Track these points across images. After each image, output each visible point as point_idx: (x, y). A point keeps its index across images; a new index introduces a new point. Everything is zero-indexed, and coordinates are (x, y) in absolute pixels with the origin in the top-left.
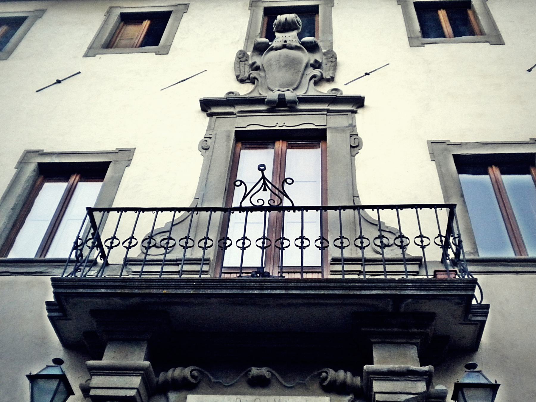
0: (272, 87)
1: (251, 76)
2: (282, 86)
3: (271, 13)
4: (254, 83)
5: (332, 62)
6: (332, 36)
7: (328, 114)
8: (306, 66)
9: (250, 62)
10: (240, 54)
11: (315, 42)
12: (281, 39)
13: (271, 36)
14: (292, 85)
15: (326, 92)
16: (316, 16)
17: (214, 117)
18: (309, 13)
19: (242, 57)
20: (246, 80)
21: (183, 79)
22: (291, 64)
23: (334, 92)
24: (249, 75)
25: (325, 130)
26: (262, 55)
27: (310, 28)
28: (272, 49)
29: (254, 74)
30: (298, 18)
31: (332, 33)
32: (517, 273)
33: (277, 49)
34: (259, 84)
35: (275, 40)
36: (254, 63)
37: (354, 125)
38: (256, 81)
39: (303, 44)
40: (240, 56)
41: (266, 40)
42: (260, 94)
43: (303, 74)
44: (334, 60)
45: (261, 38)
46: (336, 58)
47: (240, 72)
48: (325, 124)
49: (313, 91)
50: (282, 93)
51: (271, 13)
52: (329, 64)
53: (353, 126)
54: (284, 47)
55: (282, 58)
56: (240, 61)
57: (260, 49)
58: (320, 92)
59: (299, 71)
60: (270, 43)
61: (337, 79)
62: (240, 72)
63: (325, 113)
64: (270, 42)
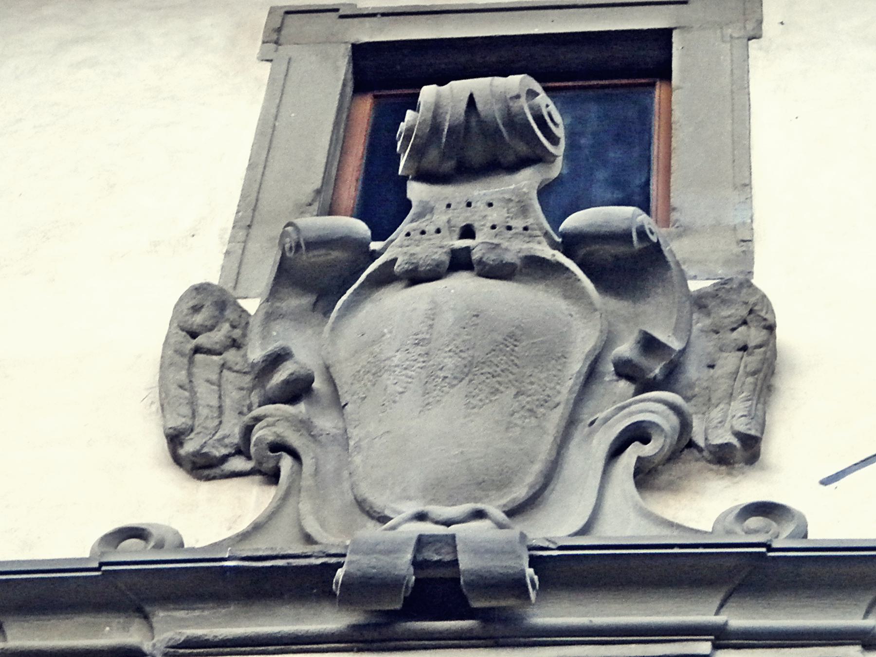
0: (379, 500)
1: (258, 433)
2: (439, 488)
3: (385, 73)
4: (273, 477)
5: (744, 348)
6: (749, 199)
8: (592, 374)
9: (256, 353)
10: (196, 309)
11: (642, 234)
12: (440, 218)
13: (384, 206)
14: (502, 483)
15: (706, 525)
16: (659, 92)
18: (617, 77)
19: (204, 324)
20: (225, 458)
22: (498, 360)
23: (754, 522)
24: (248, 431)
26: (327, 313)
27: (626, 156)
28: (386, 277)
29: (277, 421)
30: (543, 99)
31: (747, 185)
33: (415, 277)
34: (307, 480)
35: (405, 226)
36: (277, 359)
38: (286, 463)
39: (570, 244)
40: (198, 319)
41: (361, 228)
42: (309, 539)
43: (571, 423)
44: (754, 335)
45: (331, 210)
46: (771, 328)
47: (194, 415)
49: (627, 520)
50: (441, 530)
51: (385, 73)
52: (729, 361)
54: (460, 262)
55: (448, 318)
56: (197, 350)
57: (319, 277)
58: (671, 525)
60: (375, 246)
61: (777, 446)
62: (194, 415)
64: (375, 237)
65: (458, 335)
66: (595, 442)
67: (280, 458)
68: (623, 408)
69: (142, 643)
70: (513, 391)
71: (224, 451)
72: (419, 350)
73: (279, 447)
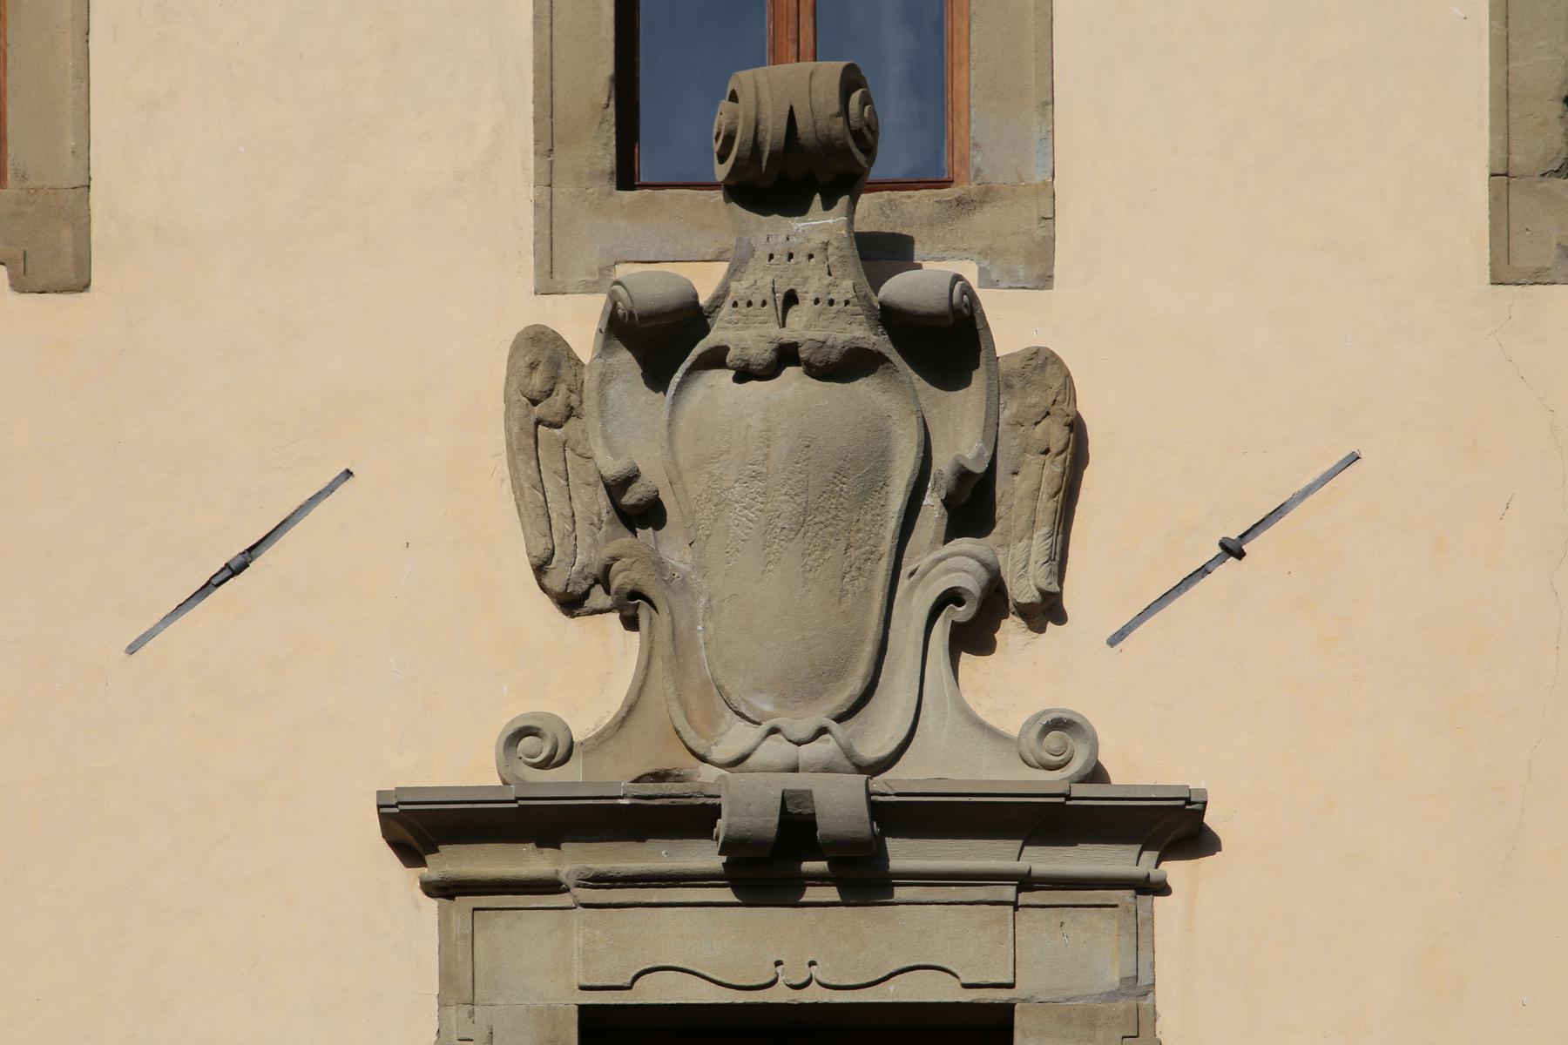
7: (1025, 898)
10: (533, 366)
14: (837, 673)
17: (466, 903)
20: (586, 595)
21: (231, 551)
25: (1007, 1010)
32: (670, 797)
37: (1144, 980)
38: (644, 612)
48: (1009, 980)
53: (1138, 987)
59: (871, 556)
63: (1009, 892)
65: (792, 472)
66: (915, 600)
67: (637, 606)
68: (940, 560)
69: (557, 872)
70: (842, 545)
71: (585, 586)
72: (758, 485)
73: (636, 594)
